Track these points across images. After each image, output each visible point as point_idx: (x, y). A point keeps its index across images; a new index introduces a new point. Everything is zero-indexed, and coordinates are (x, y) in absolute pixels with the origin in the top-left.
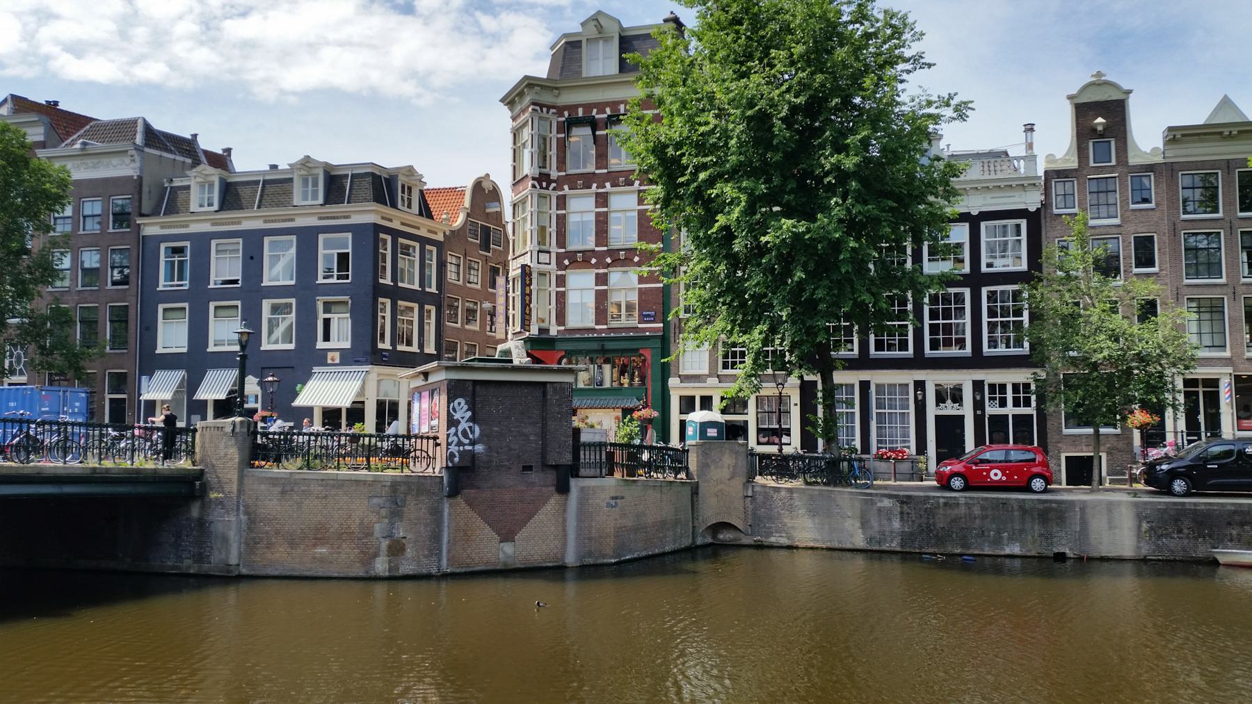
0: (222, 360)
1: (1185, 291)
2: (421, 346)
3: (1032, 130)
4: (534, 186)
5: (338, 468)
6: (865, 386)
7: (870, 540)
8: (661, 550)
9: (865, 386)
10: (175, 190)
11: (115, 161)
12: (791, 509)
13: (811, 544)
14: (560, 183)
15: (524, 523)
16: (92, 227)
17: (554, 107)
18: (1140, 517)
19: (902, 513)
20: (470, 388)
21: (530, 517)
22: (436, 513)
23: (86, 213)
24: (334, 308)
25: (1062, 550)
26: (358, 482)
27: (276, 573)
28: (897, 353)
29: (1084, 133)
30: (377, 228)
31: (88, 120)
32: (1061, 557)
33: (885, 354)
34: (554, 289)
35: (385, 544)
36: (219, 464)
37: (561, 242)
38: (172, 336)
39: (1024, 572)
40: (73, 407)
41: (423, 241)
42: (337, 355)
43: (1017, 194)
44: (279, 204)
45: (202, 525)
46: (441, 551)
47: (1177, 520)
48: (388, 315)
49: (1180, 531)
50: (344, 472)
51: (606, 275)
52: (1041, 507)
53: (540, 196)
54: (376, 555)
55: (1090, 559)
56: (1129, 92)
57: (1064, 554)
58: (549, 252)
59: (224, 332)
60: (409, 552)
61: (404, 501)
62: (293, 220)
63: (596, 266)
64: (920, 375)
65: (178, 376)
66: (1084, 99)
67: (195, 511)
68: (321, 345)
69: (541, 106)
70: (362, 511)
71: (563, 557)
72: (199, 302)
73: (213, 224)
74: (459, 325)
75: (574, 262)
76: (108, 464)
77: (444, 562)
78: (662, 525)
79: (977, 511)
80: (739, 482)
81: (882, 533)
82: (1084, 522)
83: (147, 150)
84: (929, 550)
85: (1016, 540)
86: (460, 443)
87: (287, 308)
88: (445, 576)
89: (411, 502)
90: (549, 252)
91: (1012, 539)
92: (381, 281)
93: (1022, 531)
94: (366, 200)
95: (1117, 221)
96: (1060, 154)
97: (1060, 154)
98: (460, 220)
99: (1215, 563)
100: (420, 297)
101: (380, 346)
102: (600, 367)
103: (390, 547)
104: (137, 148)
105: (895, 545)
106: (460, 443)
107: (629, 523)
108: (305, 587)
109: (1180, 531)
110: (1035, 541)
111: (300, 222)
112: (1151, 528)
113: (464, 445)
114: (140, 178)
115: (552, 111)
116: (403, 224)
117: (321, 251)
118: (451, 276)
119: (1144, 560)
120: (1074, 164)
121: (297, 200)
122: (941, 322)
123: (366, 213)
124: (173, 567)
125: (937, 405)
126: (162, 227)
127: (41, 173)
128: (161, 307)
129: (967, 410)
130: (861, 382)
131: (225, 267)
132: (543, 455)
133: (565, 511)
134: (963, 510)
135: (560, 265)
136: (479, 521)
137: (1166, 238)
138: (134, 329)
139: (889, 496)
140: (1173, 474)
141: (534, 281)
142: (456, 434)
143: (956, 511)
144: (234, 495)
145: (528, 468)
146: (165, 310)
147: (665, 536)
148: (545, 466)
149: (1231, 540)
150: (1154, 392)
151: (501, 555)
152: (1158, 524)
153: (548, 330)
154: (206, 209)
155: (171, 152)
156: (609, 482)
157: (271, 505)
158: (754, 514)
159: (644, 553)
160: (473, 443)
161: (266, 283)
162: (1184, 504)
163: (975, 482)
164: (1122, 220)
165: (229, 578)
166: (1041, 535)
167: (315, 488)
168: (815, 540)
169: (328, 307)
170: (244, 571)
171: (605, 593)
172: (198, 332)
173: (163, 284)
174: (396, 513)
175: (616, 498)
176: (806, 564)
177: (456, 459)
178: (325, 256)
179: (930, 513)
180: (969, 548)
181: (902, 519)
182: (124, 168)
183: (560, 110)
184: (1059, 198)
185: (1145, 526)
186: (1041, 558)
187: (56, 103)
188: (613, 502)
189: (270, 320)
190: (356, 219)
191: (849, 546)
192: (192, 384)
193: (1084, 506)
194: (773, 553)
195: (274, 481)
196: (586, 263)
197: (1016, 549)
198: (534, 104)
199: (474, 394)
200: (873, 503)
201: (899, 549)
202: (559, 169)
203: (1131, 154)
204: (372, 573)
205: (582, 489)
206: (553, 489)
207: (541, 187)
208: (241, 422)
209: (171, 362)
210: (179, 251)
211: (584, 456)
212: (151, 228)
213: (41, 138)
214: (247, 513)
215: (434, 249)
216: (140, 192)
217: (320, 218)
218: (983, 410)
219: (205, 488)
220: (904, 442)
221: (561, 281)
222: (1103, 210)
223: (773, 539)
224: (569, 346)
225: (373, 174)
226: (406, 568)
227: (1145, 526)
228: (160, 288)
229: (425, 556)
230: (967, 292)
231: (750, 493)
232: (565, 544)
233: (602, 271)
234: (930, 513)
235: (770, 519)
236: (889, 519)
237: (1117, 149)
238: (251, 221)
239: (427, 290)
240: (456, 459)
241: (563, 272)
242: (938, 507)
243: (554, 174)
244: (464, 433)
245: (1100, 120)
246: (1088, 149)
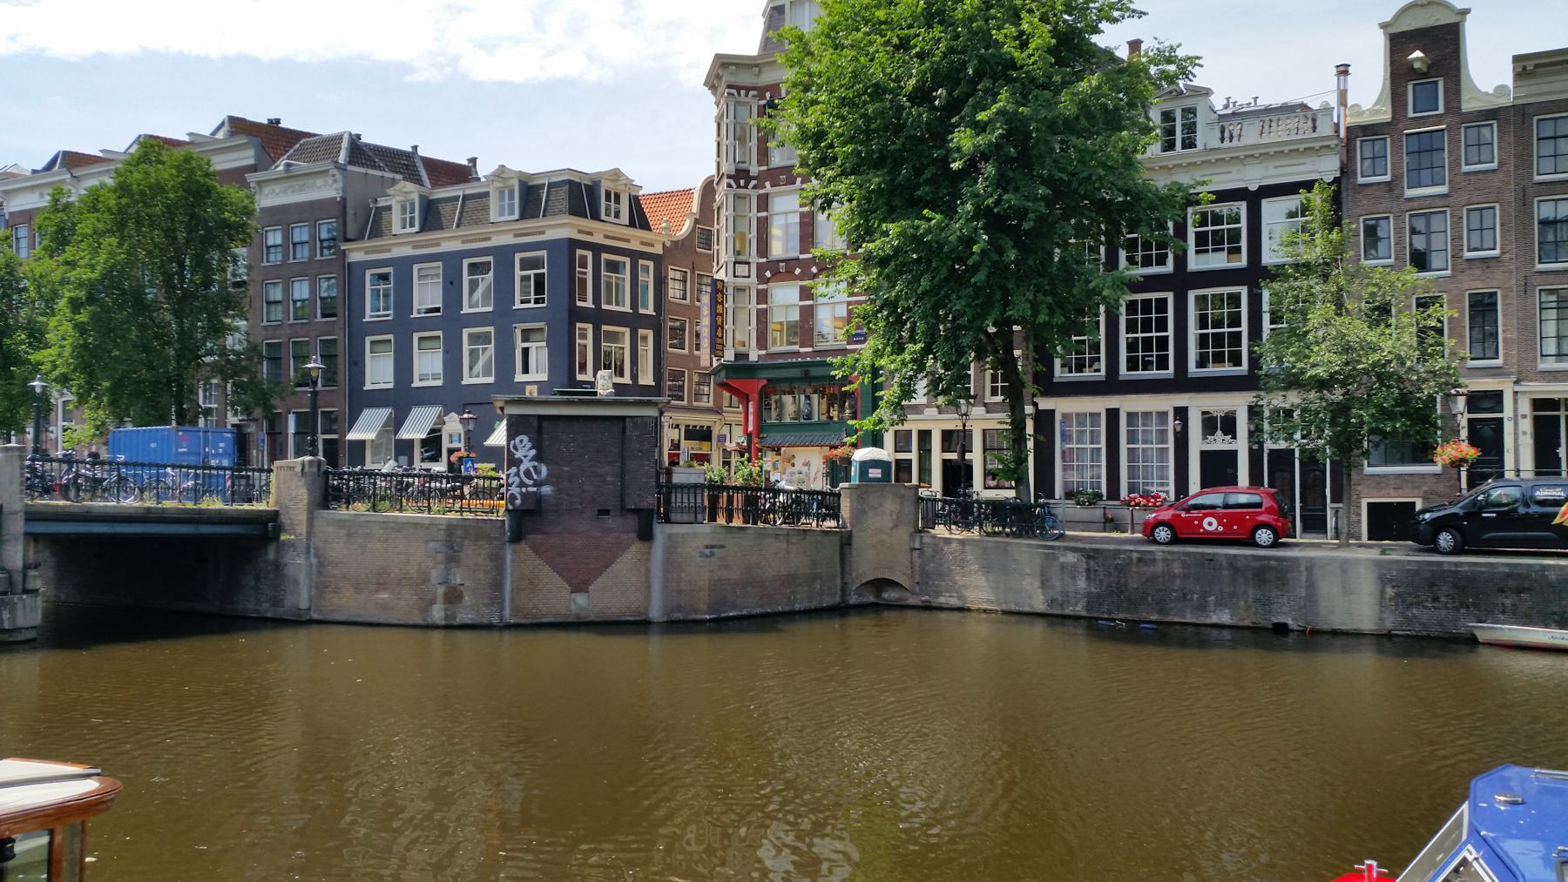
0: (426, 397)
1: (1535, 280)
2: (634, 376)
3: (1346, 73)
4: (729, 186)
6: (1113, 415)
7: (1052, 602)
8: (787, 608)
9: (1113, 415)
10: (379, 211)
12: (963, 563)
13: (985, 606)
14: (762, 179)
16: (303, 254)
17: (754, 88)
18: (1383, 581)
19: (1088, 570)
21: (607, 565)
22: (497, 560)
23: (297, 239)
24: (533, 336)
25: (1281, 619)
26: (416, 525)
27: (342, 618)
28: (1154, 373)
29: (1399, 73)
30: (573, 244)
31: (295, 136)
32: (1281, 629)
33: (1140, 374)
34: (754, 306)
35: (441, 590)
37: (763, 248)
38: (379, 372)
39: (1234, 644)
40: (217, 448)
41: (635, 256)
42: (534, 388)
43: (1306, 160)
45: (277, 566)
46: (503, 601)
47: (1432, 585)
48: (589, 342)
49: (1435, 599)
50: (409, 514)
52: (1257, 564)
54: (433, 602)
55: (1316, 633)
56: (1465, 12)
57: (1285, 625)
59: (428, 366)
62: (542, 233)
63: (801, 277)
64: (1180, 400)
65: (383, 414)
66: (1404, 27)
67: (271, 554)
68: (520, 377)
69: (738, 89)
70: (422, 557)
72: (402, 330)
73: (415, 247)
74: (686, 351)
75: (776, 273)
76: (168, 504)
77: (507, 612)
78: (791, 579)
79: (1177, 568)
80: (903, 533)
81: (1065, 594)
82: (1311, 586)
83: (350, 168)
84: (1122, 616)
85: (1226, 606)
86: (522, 484)
87: (484, 338)
91: (1220, 605)
92: (579, 304)
93: (1233, 595)
95: (1443, 189)
96: (1367, 104)
97: (1367, 104)
98: (687, 226)
99: (1472, 642)
100: (634, 321)
103: (446, 594)
104: (341, 168)
105: (1079, 609)
106: (522, 484)
107: (735, 575)
108: (369, 630)
109: (1435, 599)
110: (1248, 608)
111: (397, 252)
112: (1398, 595)
114: (344, 199)
115: (752, 93)
116: (606, 237)
117: (518, 273)
118: (674, 291)
119: (1389, 636)
120: (1386, 115)
121: (494, 216)
122: (1154, 334)
123: (561, 227)
124: (255, 611)
125: (1205, 438)
126: (464, 242)
127: (221, 203)
128: (368, 340)
129: (1241, 446)
130: (1176, 409)
131: (427, 295)
133: (648, 560)
134: (1160, 567)
135: (761, 279)
136: (547, 569)
137: (1512, 211)
138: (344, 365)
139: (1074, 550)
140: (1440, 525)
141: (730, 298)
142: (517, 474)
143: (1152, 569)
144: (303, 537)
145: (604, 512)
146: (373, 343)
147: (794, 593)
148: (624, 510)
149: (1504, 612)
150: (1390, 419)
151: (573, 607)
152: (1406, 589)
154: (409, 230)
155: (379, 168)
156: (705, 528)
157: (338, 549)
158: (922, 567)
159: (758, 611)
160: (538, 484)
161: (466, 310)
162: (1440, 564)
163: (1184, 533)
164: (1451, 188)
166: (1256, 600)
167: (378, 531)
168: (988, 601)
170: (315, 616)
171: (699, 646)
172: (404, 367)
174: (452, 559)
175: (713, 547)
176: (978, 629)
177: (518, 502)
179: (1121, 570)
180: (1167, 615)
181: (1088, 578)
182: (327, 190)
183: (761, 91)
184: (1367, 163)
185: (1390, 592)
186: (1255, 629)
187: (278, 121)
188: (707, 551)
191: (1027, 609)
192: (397, 422)
193: (1311, 565)
194: (943, 615)
195: (341, 523)
196: (789, 275)
197: (1225, 617)
198: (729, 87)
199: (540, 430)
200: (1055, 558)
201: (1084, 613)
202: (760, 163)
203: (1465, 96)
204: (430, 621)
205: (670, 536)
206: (634, 535)
207: (739, 186)
208: (310, 462)
209: (378, 399)
210: (384, 278)
211: (678, 499)
213: (251, 161)
214: (317, 556)
215: (651, 264)
217: (516, 236)
218: (1261, 444)
219: (279, 529)
220: (1162, 484)
221: (763, 297)
222: (1426, 174)
223: (942, 600)
225: (571, 183)
226: (464, 617)
227: (1390, 592)
228: (367, 319)
229: (486, 605)
230: (1244, 291)
231: (917, 545)
232: (648, 597)
233: (807, 283)
234: (1121, 570)
235: (940, 575)
236: (1074, 578)
237: (1446, 92)
238: (449, 242)
239: (641, 311)
240: (518, 502)
242: (1130, 563)
243: (754, 169)
244: (528, 473)
245: (1418, 54)
246: (1406, 94)
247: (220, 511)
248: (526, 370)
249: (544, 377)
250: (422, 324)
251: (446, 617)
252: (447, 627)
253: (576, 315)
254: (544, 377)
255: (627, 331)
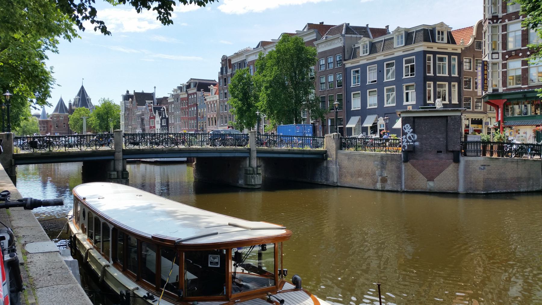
0: (372, 112)
4: (489, 23)
5: (365, 150)
8: (517, 191)
11: (336, 41)
15: (438, 174)
20: (412, 120)
22: (399, 168)
24: (410, 88)
26: (370, 156)
30: (425, 52)
34: (501, 70)
35: (380, 178)
36: (330, 148)
38: (356, 104)
41: (450, 54)
42: (411, 107)
44: (390, 48)
45: (327, 168)
48: (432, 89)
50: (368, 152)
51: (506, 63)
53: (493, 27)
54: (377, 182)
58: (498, 53)
59: (372, 101)
60: (389, 182)
61: (386, 163)
62: (413, 49)
63: (522, 57)
68: (405, 103)
70: (373, 166)
71: (457, 189)
72: (363, 90)
73: (367, 60)
76: (295, 148)
77: (403, 187)
78: (519, 179)
83: (346, 35)
86: (407, 142)
87: (392, 90)
88: (404, 192)
89: (389, 164)
90: (498, 53)
92: (428, 74)
94: (421, 41)
100: (449, 79)
101: (428, 102)
102: (526, 106)
103: (381, 179)
106: (407, 142)
107: (494, 177)
111: (397, 54)
113: (409, 142)
114: (344, 46)
116: (438, 48)
121: (395, 46)
127: (307, 52)
131: (372, 76)
132: (447, 146)
133: (458, 170)
135: (504, 59)
141: (490, 68)
142: (406, 138)
148: (448, 151)
153: (497, 90)
154: (365, 54)
155: (354, 34)
157: (345, 163)
159: (505, 191)
165: (335, 186)
167: (358, 158)
169: (407, 88)
170: (339, 184)
171: (479, 204)
172: (364, 102)
173: (352, 85)
174: (383, 167)
175: (485, 166)
177: (406, 148)
178: (406, 67)
182: (338, 44)
187: (323, 23)
188: (482, 167)
189: (387, 95)
190: (417, 50)
192: (362, 121)
195: (346, 155)
199: (414, 122)
202: (503, 12)
204: (376, 188)
205: (466, 161)
206: (452, 161)
207: (493, 23)
209: (356, 113)
210: (357, 72)
211: (469, 147)
212: (348, 65)
213: (315, 37)
214: (339, 165)
216: (344, 52)
217: (403, 52)
219: (327, 156)
221: (505, 66)
224: (508, 97)
225: (424, 29)
226: (388, 187)
232: (458, 184)
233: (525, 59)
238: (379, 57)
239: (453, 75)
240: (406, 148)
241: (505, 62)
243: (500, 15)
244: (410, 138)
247: (310, 150)
248: (407, 100)
249: (414, 103)
250: (370, 87)
251: (382, 187)
252: (382, 191)
253: (426, 79)
254: (414, 103)
255: (447, 83)
